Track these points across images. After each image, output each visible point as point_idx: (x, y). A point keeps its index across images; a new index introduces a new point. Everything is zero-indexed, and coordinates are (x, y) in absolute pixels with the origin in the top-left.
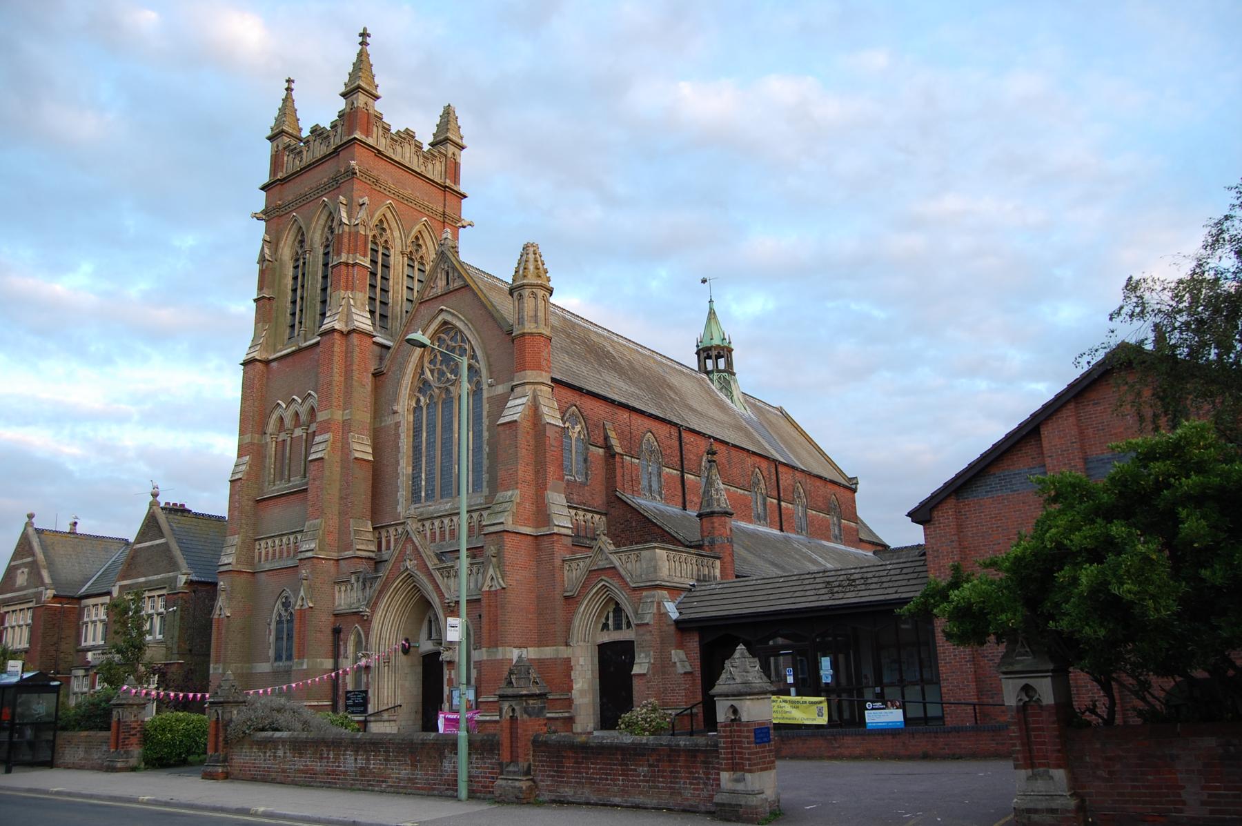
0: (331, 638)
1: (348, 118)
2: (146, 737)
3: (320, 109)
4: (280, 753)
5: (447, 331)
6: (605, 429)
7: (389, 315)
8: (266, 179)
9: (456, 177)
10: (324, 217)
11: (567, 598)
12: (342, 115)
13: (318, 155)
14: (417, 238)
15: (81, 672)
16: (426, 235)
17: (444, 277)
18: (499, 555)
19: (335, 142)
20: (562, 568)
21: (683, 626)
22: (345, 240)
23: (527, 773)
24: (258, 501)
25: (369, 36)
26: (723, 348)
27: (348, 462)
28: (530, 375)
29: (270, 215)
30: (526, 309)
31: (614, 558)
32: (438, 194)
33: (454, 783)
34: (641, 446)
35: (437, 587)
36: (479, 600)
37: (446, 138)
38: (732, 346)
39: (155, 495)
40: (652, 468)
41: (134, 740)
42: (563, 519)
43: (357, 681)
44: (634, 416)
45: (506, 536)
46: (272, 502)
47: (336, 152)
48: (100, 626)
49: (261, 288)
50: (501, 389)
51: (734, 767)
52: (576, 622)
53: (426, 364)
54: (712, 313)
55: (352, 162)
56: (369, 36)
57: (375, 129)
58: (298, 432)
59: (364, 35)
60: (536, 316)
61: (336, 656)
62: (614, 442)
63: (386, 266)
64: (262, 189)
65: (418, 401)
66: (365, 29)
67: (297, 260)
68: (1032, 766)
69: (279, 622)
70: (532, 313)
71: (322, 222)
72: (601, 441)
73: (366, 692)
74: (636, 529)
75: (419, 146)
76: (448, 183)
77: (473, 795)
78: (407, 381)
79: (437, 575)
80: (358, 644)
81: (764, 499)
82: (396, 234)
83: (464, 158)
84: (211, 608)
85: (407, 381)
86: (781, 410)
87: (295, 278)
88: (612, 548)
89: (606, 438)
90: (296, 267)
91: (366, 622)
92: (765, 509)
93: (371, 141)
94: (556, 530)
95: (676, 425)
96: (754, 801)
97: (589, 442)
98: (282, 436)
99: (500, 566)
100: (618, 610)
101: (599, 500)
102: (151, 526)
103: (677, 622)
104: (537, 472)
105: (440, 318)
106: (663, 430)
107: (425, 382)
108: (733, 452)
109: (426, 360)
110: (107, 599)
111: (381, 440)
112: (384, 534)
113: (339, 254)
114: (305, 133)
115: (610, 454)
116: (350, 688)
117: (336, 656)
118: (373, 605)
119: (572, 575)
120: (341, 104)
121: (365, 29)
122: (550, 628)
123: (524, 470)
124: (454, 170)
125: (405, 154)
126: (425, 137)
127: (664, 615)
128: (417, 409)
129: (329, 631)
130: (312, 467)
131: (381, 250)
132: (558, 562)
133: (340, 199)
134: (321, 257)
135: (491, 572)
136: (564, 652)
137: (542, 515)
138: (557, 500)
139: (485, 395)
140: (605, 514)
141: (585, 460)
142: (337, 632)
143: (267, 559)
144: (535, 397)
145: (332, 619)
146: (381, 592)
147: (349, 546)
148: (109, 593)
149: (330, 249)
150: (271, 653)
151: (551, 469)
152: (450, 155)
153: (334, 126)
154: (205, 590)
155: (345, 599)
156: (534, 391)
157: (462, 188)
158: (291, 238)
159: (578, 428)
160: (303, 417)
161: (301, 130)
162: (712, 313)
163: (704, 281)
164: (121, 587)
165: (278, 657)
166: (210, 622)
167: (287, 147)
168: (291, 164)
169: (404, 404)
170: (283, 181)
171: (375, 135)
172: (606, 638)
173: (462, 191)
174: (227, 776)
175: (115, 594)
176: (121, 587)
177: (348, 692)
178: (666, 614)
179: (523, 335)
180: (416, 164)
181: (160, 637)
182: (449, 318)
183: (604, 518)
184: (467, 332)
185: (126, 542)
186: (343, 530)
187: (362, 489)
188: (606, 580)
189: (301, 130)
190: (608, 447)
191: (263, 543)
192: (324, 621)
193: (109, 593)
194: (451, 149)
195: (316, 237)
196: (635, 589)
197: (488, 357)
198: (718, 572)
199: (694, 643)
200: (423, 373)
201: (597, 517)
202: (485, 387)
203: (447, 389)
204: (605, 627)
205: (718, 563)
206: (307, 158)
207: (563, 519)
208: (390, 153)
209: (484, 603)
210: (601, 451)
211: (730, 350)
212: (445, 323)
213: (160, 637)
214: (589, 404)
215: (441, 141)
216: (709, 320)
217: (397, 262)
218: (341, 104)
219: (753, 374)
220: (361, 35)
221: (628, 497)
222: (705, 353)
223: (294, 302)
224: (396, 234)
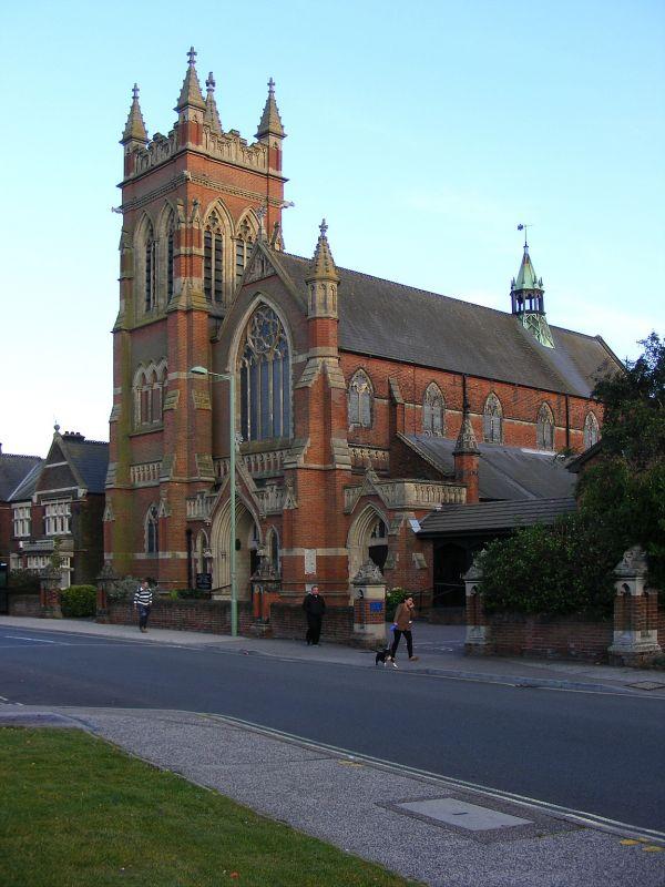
0: (185, 537)
1: (181, 129)
2: (63, 597)
3: (160, 120)
4: (287, 619)
5: (262, 310)
6: (389, 384)
7: (223, 290)
8: (121, 179)
9: (278, 167)
10: (167, 213)
11: (346, 515)
12: (176, 126)
13: (160, 161)
14: (245, 222)
15: (15, 555)
16: (252, 219)
17: (260, 265)
18: (294, 484)
19: (173, 149)
20: (342, 495)
21: (421, 537)
22: (183, 235)
23: (267, 622)
24: (131, 437)
25: (195, 54)
26: (534, 290)
27: (193, 413)
28: (320, 350)
29: (127, 209)
30: (318, 298)
31: (377, 488)
32: (262, 182)
33: (230, 627)
34: (424, 394)
35: (254, 503)
36: (280, 516)
37: (269, 129)
38: (543, 288)
39: (57, 428)
40: (437, 410)
41: (55, 600)
42: (344, 457)
43: (205, 568)
44: (419, 371)
45: (298, 472)
46: (141, 438)
47: (173, 159)
48: (26, 524)
49: (122, 270)
50: (301, 358)
51: (361, 621)
52: (352, 531)
53: (249, 335)
54: (526, 260)
55: (185, 172)
56: (195, 54)
57: (204, 135)
58: (156, 386)
59: (191, 53)
60: (325, 303)
61: (189, 550)
62: (396, 394)
63: (219, 250)
64: (119, 186)
65: (244, 363)
66: (192, 48)
67: (149, 246)
68: (475, 624)
69: (151, 525)
70: (322, 301)
71: (166, 216)
72: (386, 394)
73: (210, 575)
74: (407, 463)
75: (243, 143)
76: (272, 171)
77: (239, 633)
78: (235, 349)
79: (254, 497)
80: (204, 544)
81: (552, 428)
82: (226, 222)
83: (285, 145)
84: (102, 514)
85: (235, 349)
86: (599, 339)
87: (148, 261)
88: (377, 480)
89: (390, 391)
90: (149, 252)
91: (209, 527)
92: (552, 437)
93: (201, 148)
94: (338, 466)
95: (461, 374)
96: (368, 638)
97: (374, 396)
98: (145, 389)
99: (295, 491)
100: (382, 524)
101: (382, 437)
102: (56, 451)
103: (418, 534)
104: (325, 424)
105: (257, 299)
106: (447, 379)
107: (249, 349)
108: (520, 390)
109: (249, 331)
110: (29, 504)
111: (217, 392)
112: (222, 464)
113: (178, 248)
114: (150, 137)
115: (393, 403)
116: (200, 572)
117: (189, 550)
118: (213, 516)
119: (349, 498)
120: (175, 117)
121: (192, 48)
122: (333, 532)
123: (315, 424)
124: (275, 158)
125: (232, 154)
126: (249, 134)
127: (409, 529)
128: (243, 371)
129: (184, 532)
130: (167, 414)
131: (214, 237)
132: (339, 490)
133: (180, 185)
134: (167, 244)
135: (288, 496)
136: (342, 552)
137: (328, 455)
138: (339, 443)
139: (291, 362)
140: (388, 450)
141: (371, 410)
142: (189, 533)
143: (139, 480)
144: (324, 367)
145: (185, 524)
146: (218, 506)
147: (195, 474)
148: (30, 500)
149: (173, 239)
150: (146, 546)
151: (335, 422)
152: (272, 145)
153: (171, 135)
154: (97, 499)
155: (195, 511)
156: (323, 362)
157: (284, 174)
158: (143, 228)
159: (365, 385)
160: (159, 376)
161: (147, 132)
162: (526, 260)
163: (520, 228)
164: (38, 496)
165: (151, 550)
166: (101, 524)
167: (136, 150)
168: (141, 166)
169: (233, 365)
170: (135, 180)
171: (204, 141)
172: (375, 542)
173: (284, 176)
174: (112, 622)
175: (35, 500)
176: (38, 496)
177: (198, 575)
178: (410, 529)
179: (315, 319)
180: (241, 159)
181: (69, 532)
182: (264, 300)
183: (387, 453)
184: (276, 312)
185: (39, 459)
186: (191, 463)
187: (206, 430)
188: (372, 504)
189: (147, 132)
190: (391, 398)
191: (136, 468)
192: (179, 526)
193: (30, 500)
194: (272, 139)
195: (162, 230)
196: (390, 510)
197: (293, 333)
198: (464, 497)
199: (430, 549)
200: (246, 342)
201: (380, 453)
202: (290, 356)
203: (264, 356)
204: (374, 535)
205: (464, 490)
206: (153, 161)
207: (344, 457)
208: (217, 154)
209: (285, 518)
210: (386, 401)
211: (542, 292)
212: (262, 303)
213: (69, 532)
214: (375, 366)
215: (263, 134)
216: (524, 263)
217: (229, 245)
218: (175, 117)
219: (561, 311)
220: (189, 54)
221: (410, 441)
222: (518, 295)
223: (148, 281)
224: (226, 222)
